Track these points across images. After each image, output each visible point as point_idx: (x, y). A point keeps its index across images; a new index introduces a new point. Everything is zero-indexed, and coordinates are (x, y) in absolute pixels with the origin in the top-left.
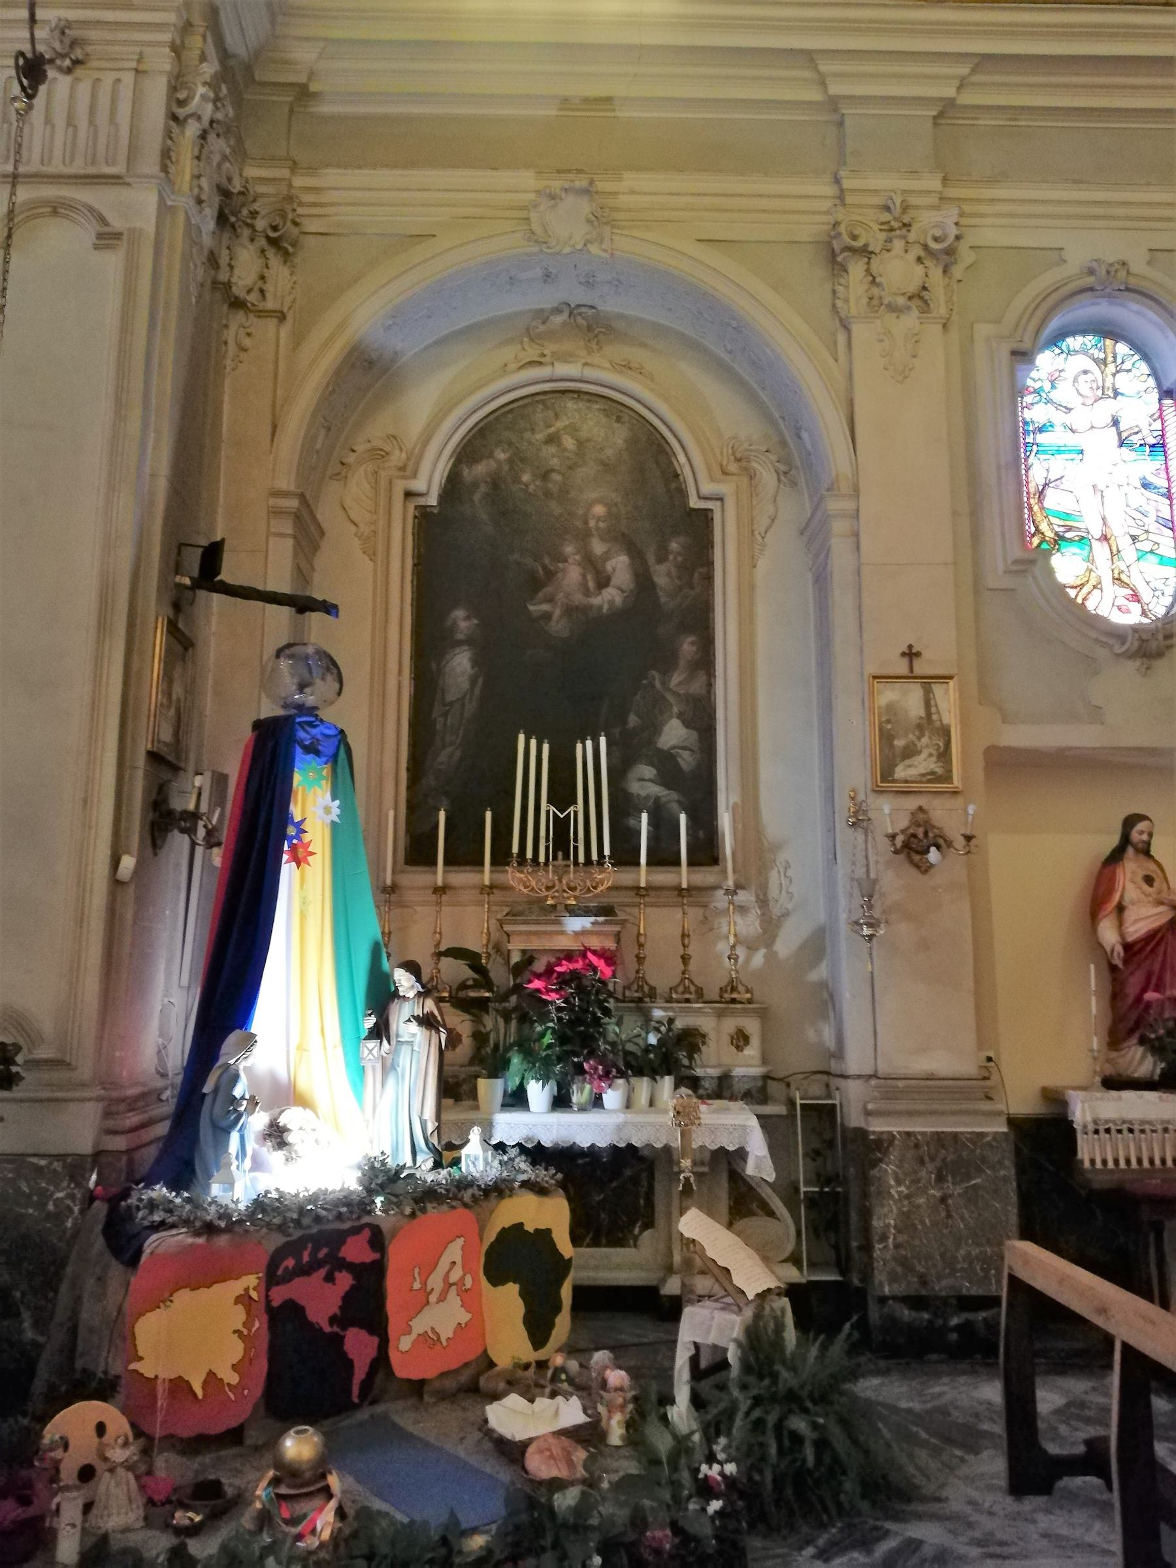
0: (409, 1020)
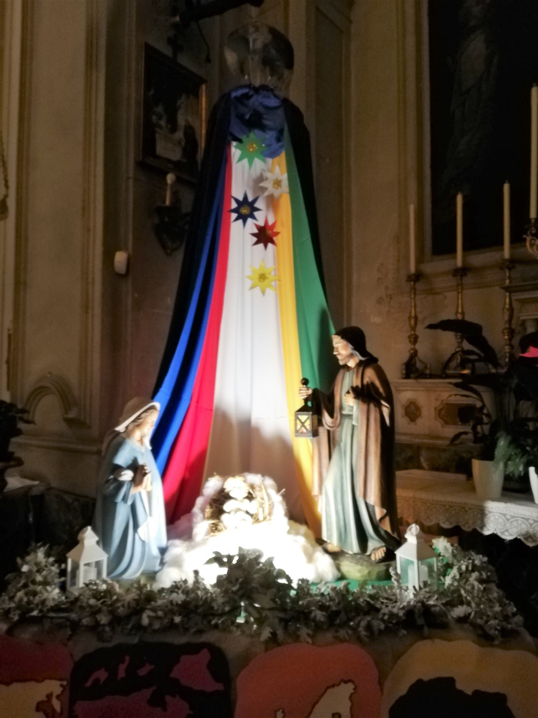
0: (348, 392)
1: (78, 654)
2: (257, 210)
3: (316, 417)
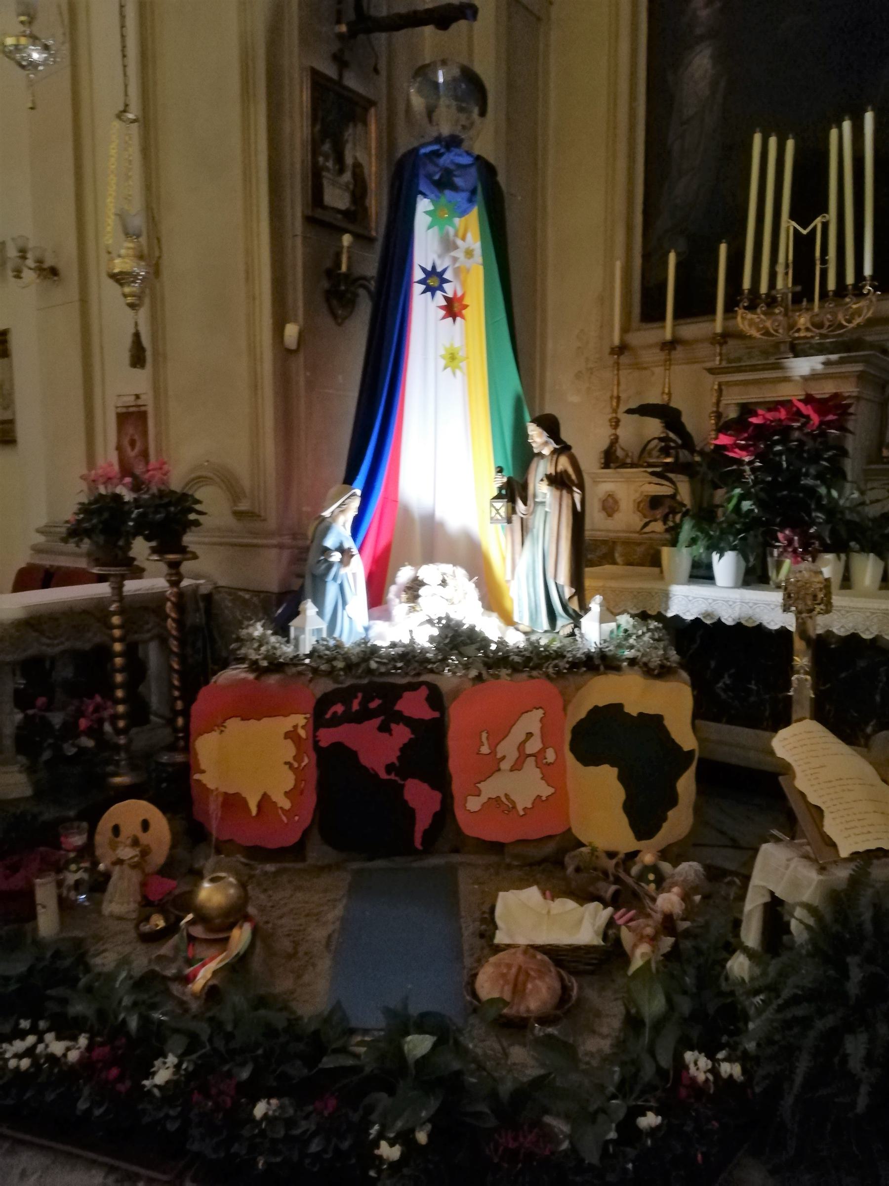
0: (542, 480)
1: (319, 695)
2: (447, 281)
3: (510, 504)
